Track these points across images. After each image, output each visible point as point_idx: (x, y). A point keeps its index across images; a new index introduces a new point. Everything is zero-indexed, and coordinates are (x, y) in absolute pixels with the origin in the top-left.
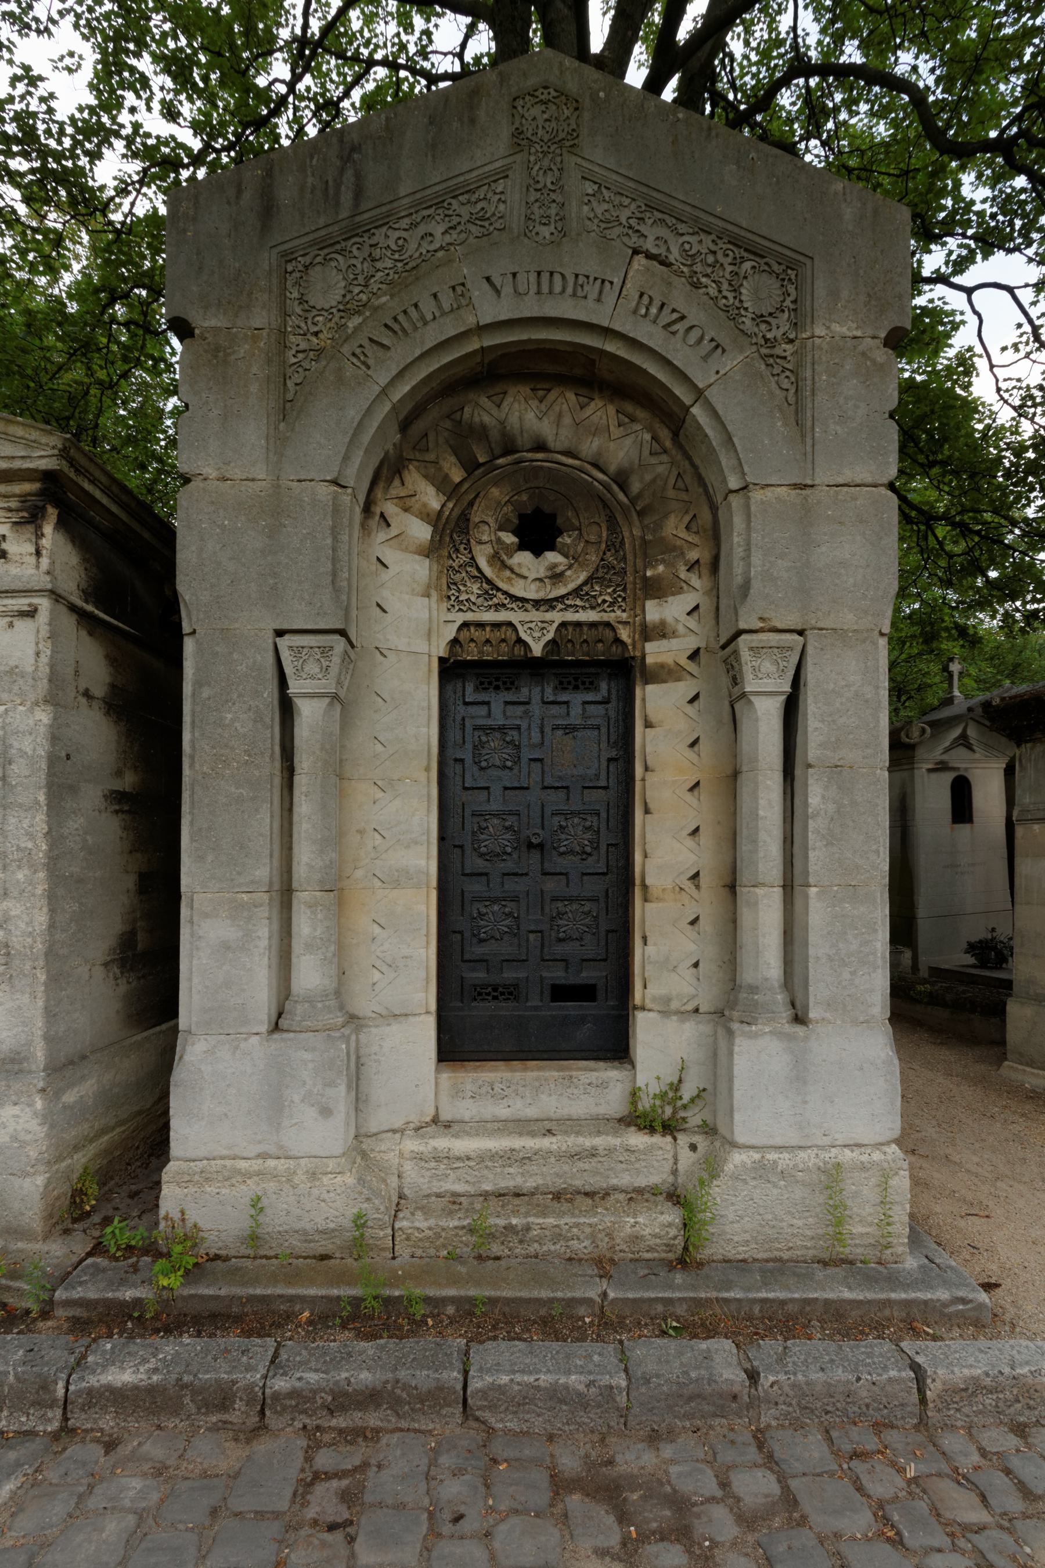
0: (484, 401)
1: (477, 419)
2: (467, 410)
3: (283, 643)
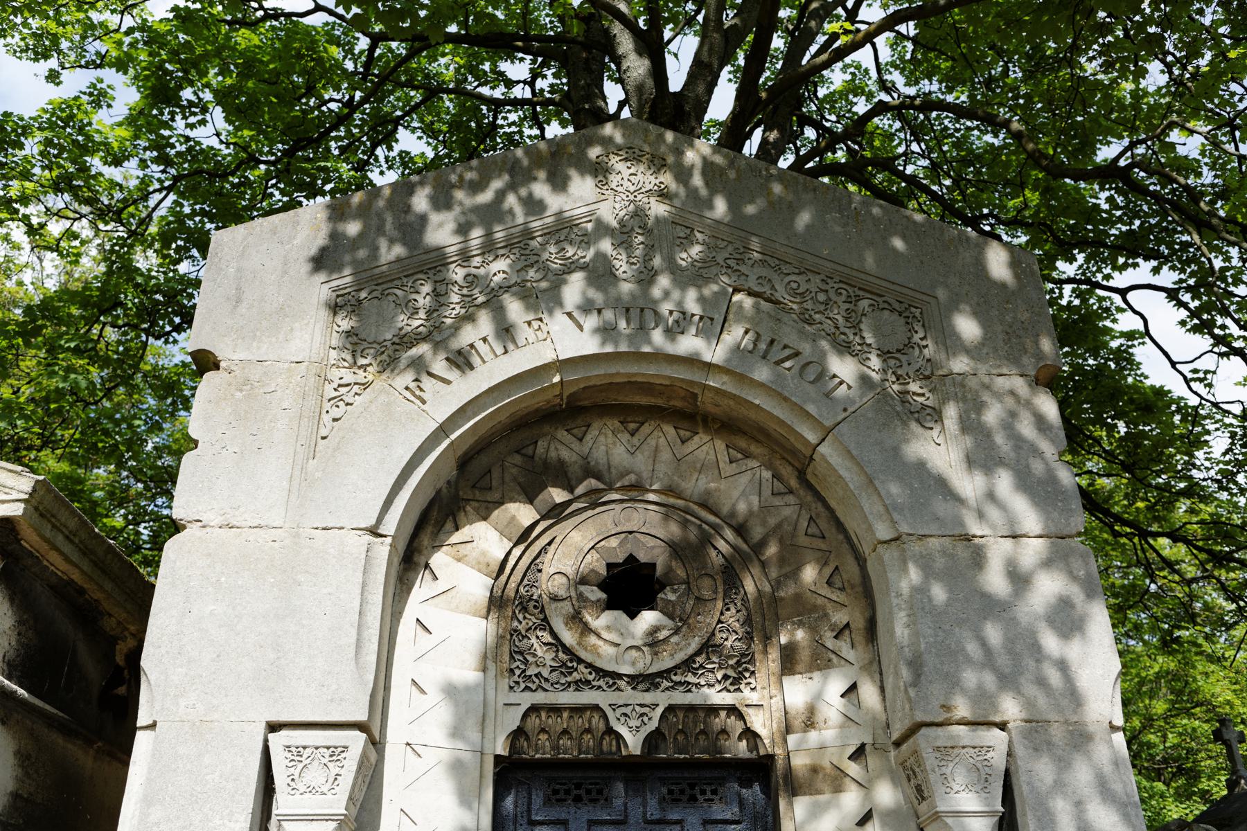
3: (278, 741)
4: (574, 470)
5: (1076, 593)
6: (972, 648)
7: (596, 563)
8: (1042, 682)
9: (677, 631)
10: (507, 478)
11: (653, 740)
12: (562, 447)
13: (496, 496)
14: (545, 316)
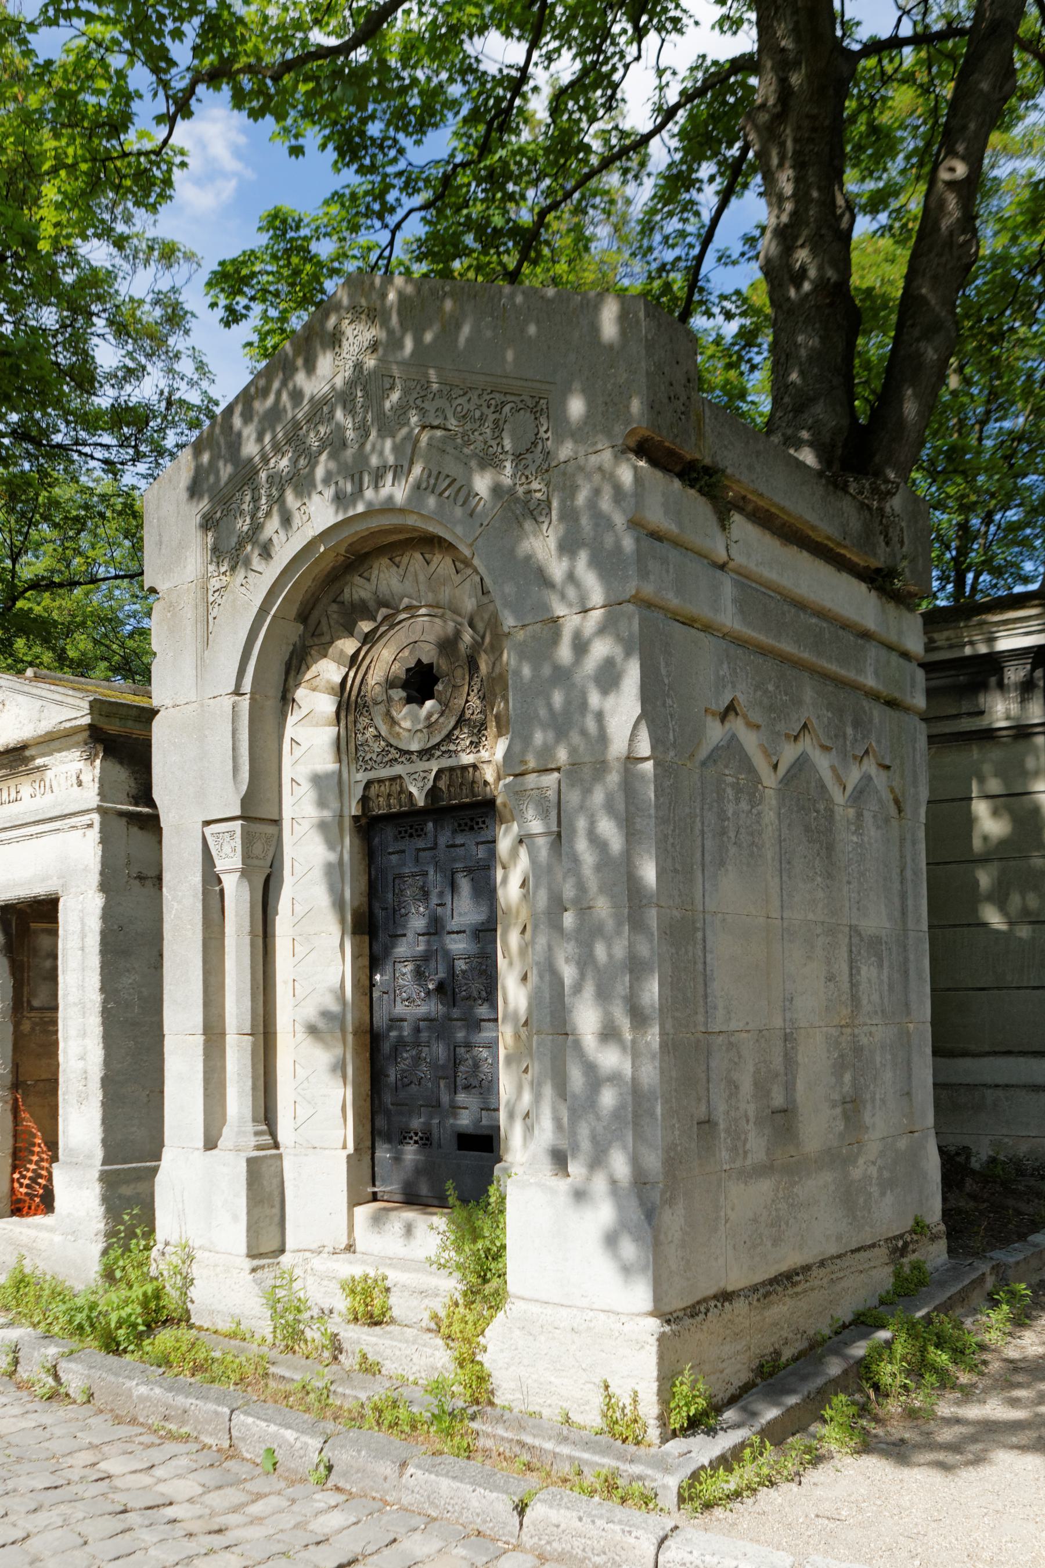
0: (357, 580)
1: (355, 597)
2: (347, 590)
3: (209, 830)
4: (372, 604)
5: (618, 651)
6: (543, 712)
7: (398, 670)
8: (584, 733)
9: (442, 714)
10: (332, 623)
11: (433, 793)
12: (359, 589)
13: (327, 638)
14: (306, 500)
